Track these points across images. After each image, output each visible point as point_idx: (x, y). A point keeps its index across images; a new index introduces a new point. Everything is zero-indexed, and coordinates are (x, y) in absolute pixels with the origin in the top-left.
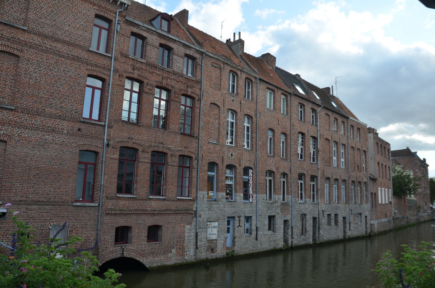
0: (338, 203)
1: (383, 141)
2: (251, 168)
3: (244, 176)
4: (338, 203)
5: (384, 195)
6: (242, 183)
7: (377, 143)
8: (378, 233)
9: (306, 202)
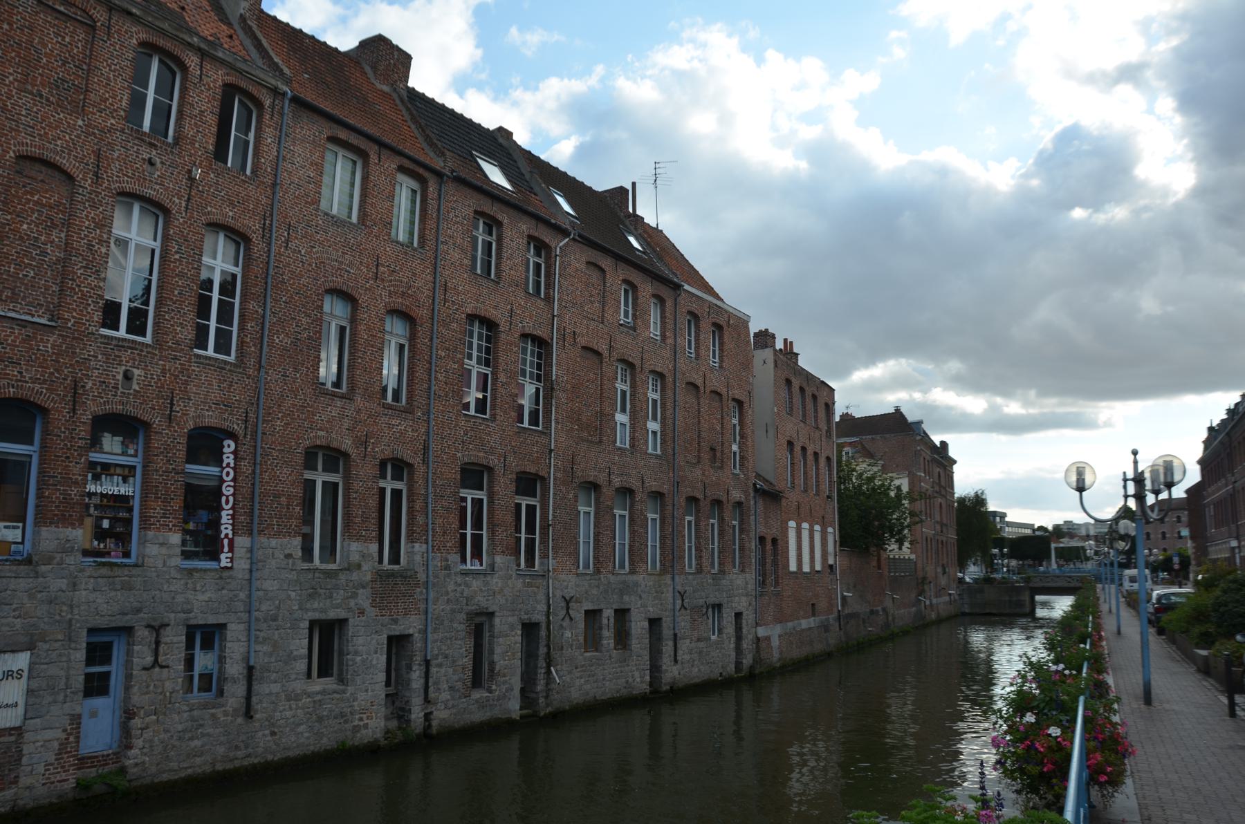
0: (633, 571)
1: (809, 377)
2: (232, 435)
3: (188, 462)
4: (633, 571)
5: (808, 546)
6: (181, 492)
7: (788, 382)
8: (783, 667)
9: (492, 566)
